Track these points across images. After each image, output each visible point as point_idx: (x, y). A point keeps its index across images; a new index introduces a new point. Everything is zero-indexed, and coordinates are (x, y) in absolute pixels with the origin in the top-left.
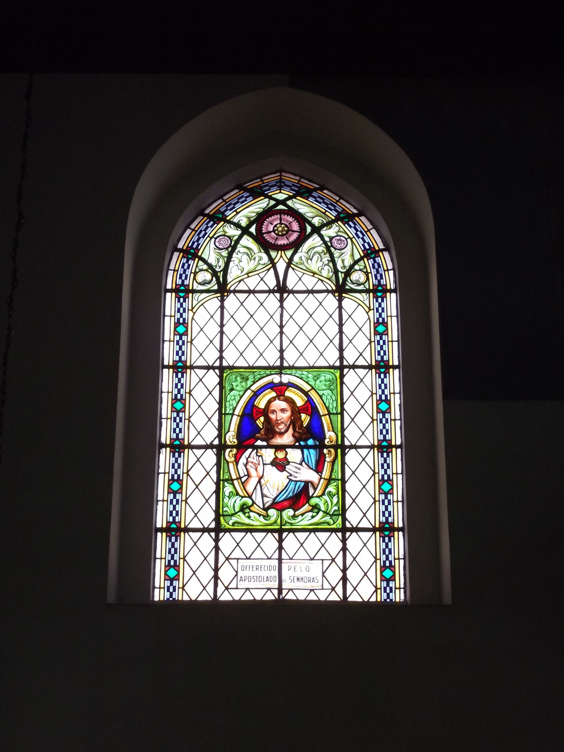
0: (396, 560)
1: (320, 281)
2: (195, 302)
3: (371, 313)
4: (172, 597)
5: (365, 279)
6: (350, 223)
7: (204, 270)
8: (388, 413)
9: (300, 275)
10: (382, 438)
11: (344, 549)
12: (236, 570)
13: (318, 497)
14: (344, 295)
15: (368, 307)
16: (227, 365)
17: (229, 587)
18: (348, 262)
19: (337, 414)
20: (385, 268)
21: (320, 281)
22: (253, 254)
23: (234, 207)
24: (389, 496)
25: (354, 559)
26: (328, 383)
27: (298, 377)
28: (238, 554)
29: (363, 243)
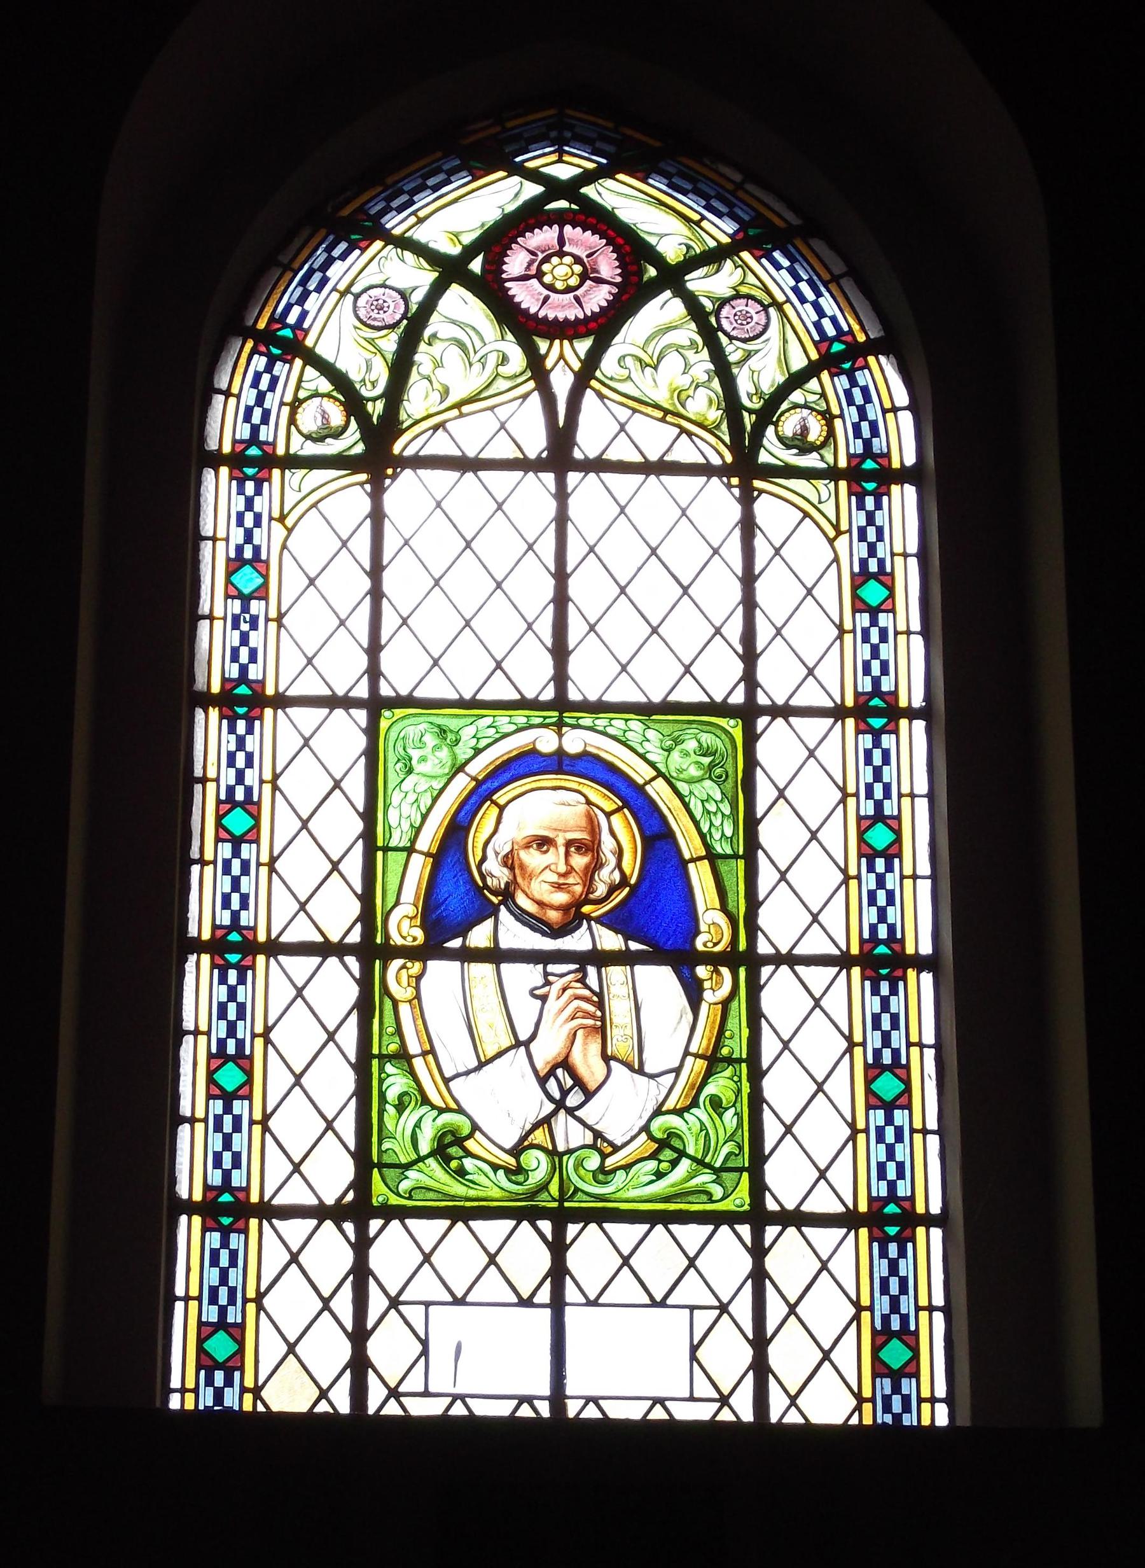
0: (921, 1313)
2: (291, 498)
4: (221, 1404)
5: (824, 434)
6: (777, 255)
7: (323, 396)
8: (903, 1109)
10: (884, 1193)
11: (759, 1276)
13: (679, 1112)
14: (757, 484)
15: (834, 522)
17: (401, 1389)
18: (771, 377)
19: (735, 856)
20: (888, 405)
22: (478, 344)
23: (412, 203)
24: (897, 1113)
25: (792, 1309)
26: (706, 760)
27: (614, 738)
28: (426, 1287)
29: (815, 318)
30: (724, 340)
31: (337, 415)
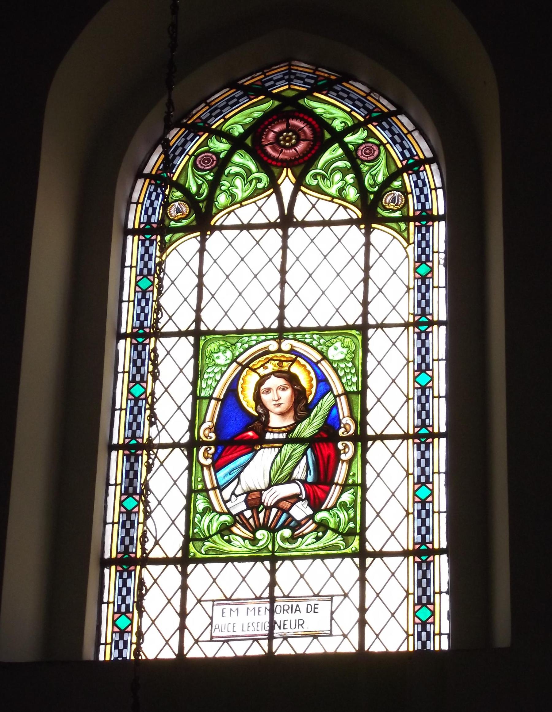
1: (341, 207)
3: (410, 249)
9: (314, 200)
12: (211, 616)
16: (206, 329)
21: (341, 207)
30: (359, 162)
31: (185, 209)
